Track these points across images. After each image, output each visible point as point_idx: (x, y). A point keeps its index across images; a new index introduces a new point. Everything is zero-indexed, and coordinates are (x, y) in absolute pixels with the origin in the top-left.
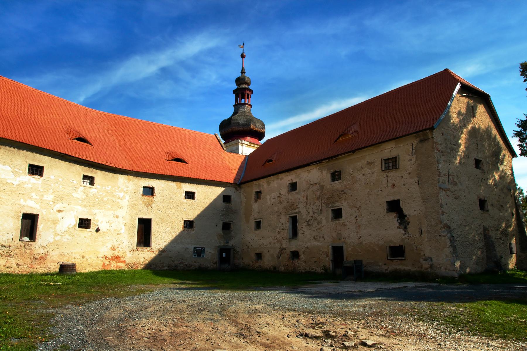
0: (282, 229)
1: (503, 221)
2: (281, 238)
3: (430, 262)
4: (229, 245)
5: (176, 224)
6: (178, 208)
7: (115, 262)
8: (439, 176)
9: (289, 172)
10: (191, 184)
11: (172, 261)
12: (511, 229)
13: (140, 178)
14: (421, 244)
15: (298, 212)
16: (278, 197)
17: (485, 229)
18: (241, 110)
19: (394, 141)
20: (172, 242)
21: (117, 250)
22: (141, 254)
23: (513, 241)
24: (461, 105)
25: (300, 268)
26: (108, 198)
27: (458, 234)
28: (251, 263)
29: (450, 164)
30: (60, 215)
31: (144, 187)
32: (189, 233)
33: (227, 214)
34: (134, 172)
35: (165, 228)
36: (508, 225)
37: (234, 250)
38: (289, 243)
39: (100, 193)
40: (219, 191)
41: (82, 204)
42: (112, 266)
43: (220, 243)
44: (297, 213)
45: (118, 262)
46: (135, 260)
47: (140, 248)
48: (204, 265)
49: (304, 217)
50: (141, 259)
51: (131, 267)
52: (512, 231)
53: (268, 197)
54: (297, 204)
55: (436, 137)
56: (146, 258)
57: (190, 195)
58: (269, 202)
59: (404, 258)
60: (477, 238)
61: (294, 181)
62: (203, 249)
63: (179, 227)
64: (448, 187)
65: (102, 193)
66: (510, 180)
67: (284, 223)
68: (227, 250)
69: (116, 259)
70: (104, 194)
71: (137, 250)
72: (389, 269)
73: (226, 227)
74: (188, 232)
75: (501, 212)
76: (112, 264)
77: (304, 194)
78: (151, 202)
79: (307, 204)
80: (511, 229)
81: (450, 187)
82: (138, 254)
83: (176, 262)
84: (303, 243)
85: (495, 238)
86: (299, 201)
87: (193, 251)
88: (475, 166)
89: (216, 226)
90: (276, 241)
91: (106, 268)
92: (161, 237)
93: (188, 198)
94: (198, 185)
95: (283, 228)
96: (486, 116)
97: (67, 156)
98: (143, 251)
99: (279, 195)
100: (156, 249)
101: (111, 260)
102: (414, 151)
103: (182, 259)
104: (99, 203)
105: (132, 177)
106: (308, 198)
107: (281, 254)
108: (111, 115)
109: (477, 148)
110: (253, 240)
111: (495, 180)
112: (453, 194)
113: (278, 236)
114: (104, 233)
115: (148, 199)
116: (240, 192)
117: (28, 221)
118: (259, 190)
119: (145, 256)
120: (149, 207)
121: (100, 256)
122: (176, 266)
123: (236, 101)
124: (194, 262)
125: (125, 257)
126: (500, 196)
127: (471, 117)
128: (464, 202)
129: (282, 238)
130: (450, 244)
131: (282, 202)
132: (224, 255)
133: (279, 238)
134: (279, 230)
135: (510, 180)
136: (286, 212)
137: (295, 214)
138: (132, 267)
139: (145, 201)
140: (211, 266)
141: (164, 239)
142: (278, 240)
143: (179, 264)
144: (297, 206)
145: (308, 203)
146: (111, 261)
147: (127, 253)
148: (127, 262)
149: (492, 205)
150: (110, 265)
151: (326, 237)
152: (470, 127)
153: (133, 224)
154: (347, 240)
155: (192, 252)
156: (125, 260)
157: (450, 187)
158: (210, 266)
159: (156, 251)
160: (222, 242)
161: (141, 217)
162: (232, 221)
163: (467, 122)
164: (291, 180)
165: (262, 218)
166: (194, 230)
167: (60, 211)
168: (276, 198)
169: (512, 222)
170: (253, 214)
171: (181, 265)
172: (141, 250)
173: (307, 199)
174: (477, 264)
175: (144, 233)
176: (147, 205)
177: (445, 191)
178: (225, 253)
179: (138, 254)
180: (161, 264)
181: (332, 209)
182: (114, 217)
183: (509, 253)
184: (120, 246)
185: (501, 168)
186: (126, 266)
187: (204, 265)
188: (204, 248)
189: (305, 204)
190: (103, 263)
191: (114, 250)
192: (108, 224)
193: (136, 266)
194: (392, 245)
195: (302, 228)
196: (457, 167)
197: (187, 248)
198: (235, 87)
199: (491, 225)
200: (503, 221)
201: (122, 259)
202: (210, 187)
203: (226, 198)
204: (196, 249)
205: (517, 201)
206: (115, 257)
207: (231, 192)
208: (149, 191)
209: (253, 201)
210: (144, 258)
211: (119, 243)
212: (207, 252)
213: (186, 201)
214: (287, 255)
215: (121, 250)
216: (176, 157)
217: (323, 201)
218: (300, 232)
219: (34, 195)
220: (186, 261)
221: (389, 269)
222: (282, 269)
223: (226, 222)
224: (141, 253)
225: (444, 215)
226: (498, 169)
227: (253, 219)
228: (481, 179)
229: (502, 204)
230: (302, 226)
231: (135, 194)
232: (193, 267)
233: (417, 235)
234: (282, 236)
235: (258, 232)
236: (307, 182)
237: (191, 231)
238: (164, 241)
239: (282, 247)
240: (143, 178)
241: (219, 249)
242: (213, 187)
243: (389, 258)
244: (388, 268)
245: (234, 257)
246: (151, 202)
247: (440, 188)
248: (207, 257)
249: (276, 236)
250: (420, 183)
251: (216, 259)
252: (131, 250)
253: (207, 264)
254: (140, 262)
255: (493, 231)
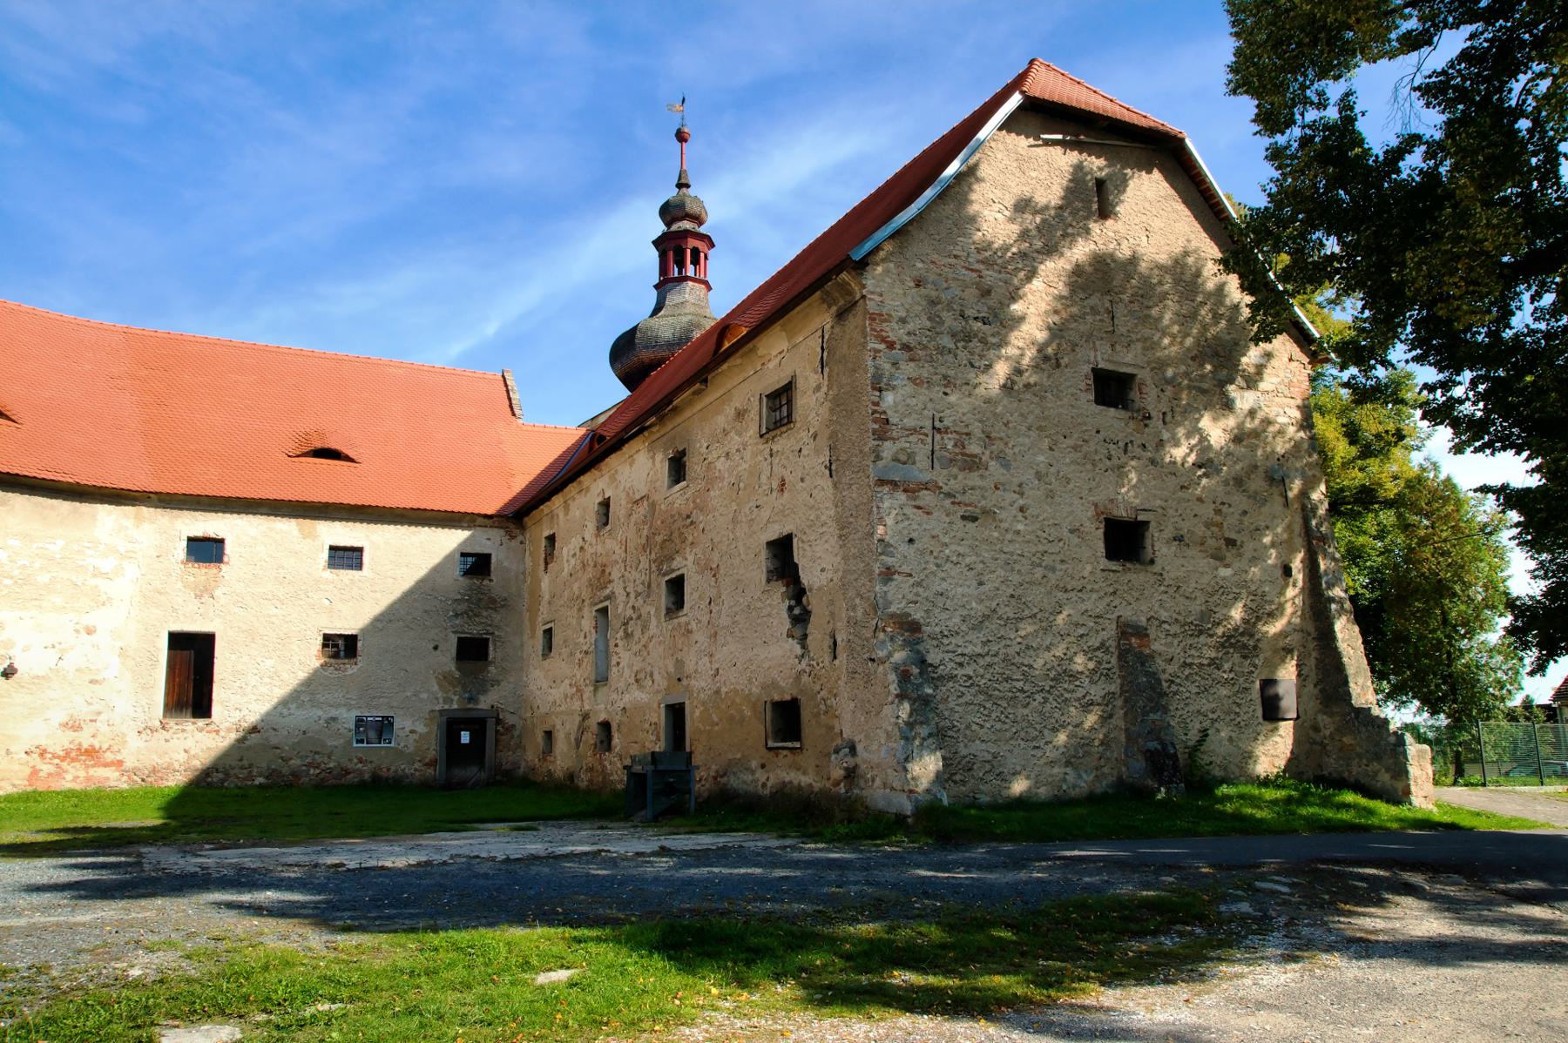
1: (1231, 596)
3: (846, 760)
4: (480, 707)
5: (295, 647)
6: (303, 596)
7: (78, 767)
8: (881, 436)
10: (350, 524)
11: (282, 758)
12: (1274, 628)
13: (176, 512)
14: (835, 691)
17: (1128, 631)
18: (673, 298)
19: (777, 328)
20: (284, 703)
21: (88, 731)
22: (175, 740)
23: (1287, 674)
24: (1034, 174)
26: (54, 574)
27: (966, 651)
29: (948, 390)
31: (190, 540)
35: (259, 660)
36: (1261, 611)
37: (498, 721)
39: (20, 563)
40: (450, 540)
42: (69, 777)
43: (447, 700)
45: (93, 766)
46: (155, 760)
47: (171, 722)
48: (393, 769)
50: (176, 756)
51: (139, 781)
52: (1283, 634)
55: (881, 295)
56: (192, 752)
57: (346, 557)
59: (797, 745)
60: (1080, 662)
63: (310, 658)
64: (926, 477)
65: (27, 563)
66: (1288, 446)
68: (477, 724)
69: (83, 758)
70: (37, 565)
71: (163, 728)
72: (769, 784)
73: (473, 651)
75: (1227, 566)
76: (66, 772)
78: (213, 584)
80: (1274, 628)
81: (940, 476)
82: (167, 741)
83: (295, 762)
85: (1185, 665)
88: (1092, 397)
91: (41, 787)
92: (244, 686)
94: (372, 526)
96: (1176, 211)
98: (183, 731)
100: (227, 724)
101: (62, 761)
102: (825, 354)
103: (316, 753)
104: (18, 590)
105: (152, 510)
109: (1111, 329)
111: (1204, 445)
112: (953, 503)
114: (36, 681)
115: (202, 572)
116: (522, 543)
117: (189, 655)
119: (190, 743)
120: (206, 598)
121: (18, 749)
122: (295, 774)
123: (664, 270)
124: (355, 761)
125: (119, 751)
126: (1223, 504)
127: (1087, 218)
128: (1018, 532)
130: (898, 691)
132: (465, 737)
135: (1292, 443)
138: (143, 780)
139: (193, 579)
140: (417, 773)
141: (255, 691)
143: (304, 768)
147: (128, 739)
148: (128, 764)
149: (1179, 539)
150: (60, 773)
151: (656, 676)
152: (1080, 251)
153: (152, 649)
154: (693, 682)
155: (350, 730)
156: (119, 757)
157: (940, 476)
158: (412, 774)
159: (229, 730)
160: (456, 698)
163: (1064, 236)
166: (356, 664)
169: (1282, 599)
171: (312, 771)
174: (1068, 763)
175: (192, 677)
176: (199, 593)
177: (905, 491)
179: (167, 741)
180: (242, 768)
181: (667, 578)
182: (77, 631)
183: (1261, 720)
184: (100, 718)
185: (1244, 400)
186: (125, 778)
187: (393, 769)
190: (28, 771)
191: (75, 731)
192: (53, 655)
193: (160, 775)
194: (777, 698)
196: (988, 401)
197: (334, 719)
198: (659, 228)
199: (1164, 615)
200: (1231, 596)
201: (109, 757)
203: (477, 565)
204: (363, 721)
205: (1314, 523)
207: (490, 542)
208: (206, 550)
210: (186, 751)
211: (94, 708)
212: (403, 728)
213: (330, 574)
215: (104, 728)
216: (319, 445)
217: (653, 556)
220: (329, 757)
221: (769, 784)
224: (175, 736)
225: (894, 583)
226: (1228, 405)
228: (1121, 444)
229: (1233, 536)
231: (161, 559)
232: (352, 775)
233: (827, 658)
236: (628, 494)
237: (348, 666)
238: (254, 697)
240: (185, 512)
241: (444, 719)
242: (426, 528)
243: (771, 744)
244: (768, 779)
245: (496, 745)
246: (213, 584)
247: (881, 482)
248: (402, 745)
250: (833, 468)
251: (433, 749)
252: (141, 729)
253: (403, 767)
254: (170, 764)
255: (1175, 635)
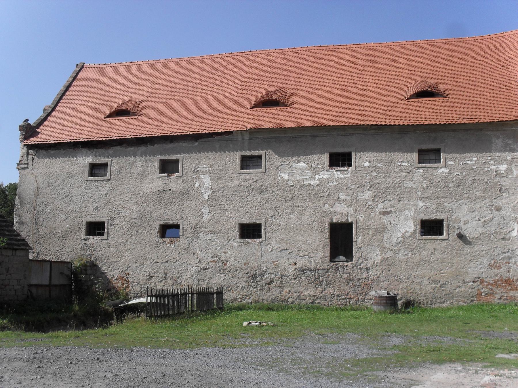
30: (385, 219)
41: (423, 196)
97: (394, 126)
146: (494, 288)
167: (385, 213)
206: (502, 280)
219: (343, 197)
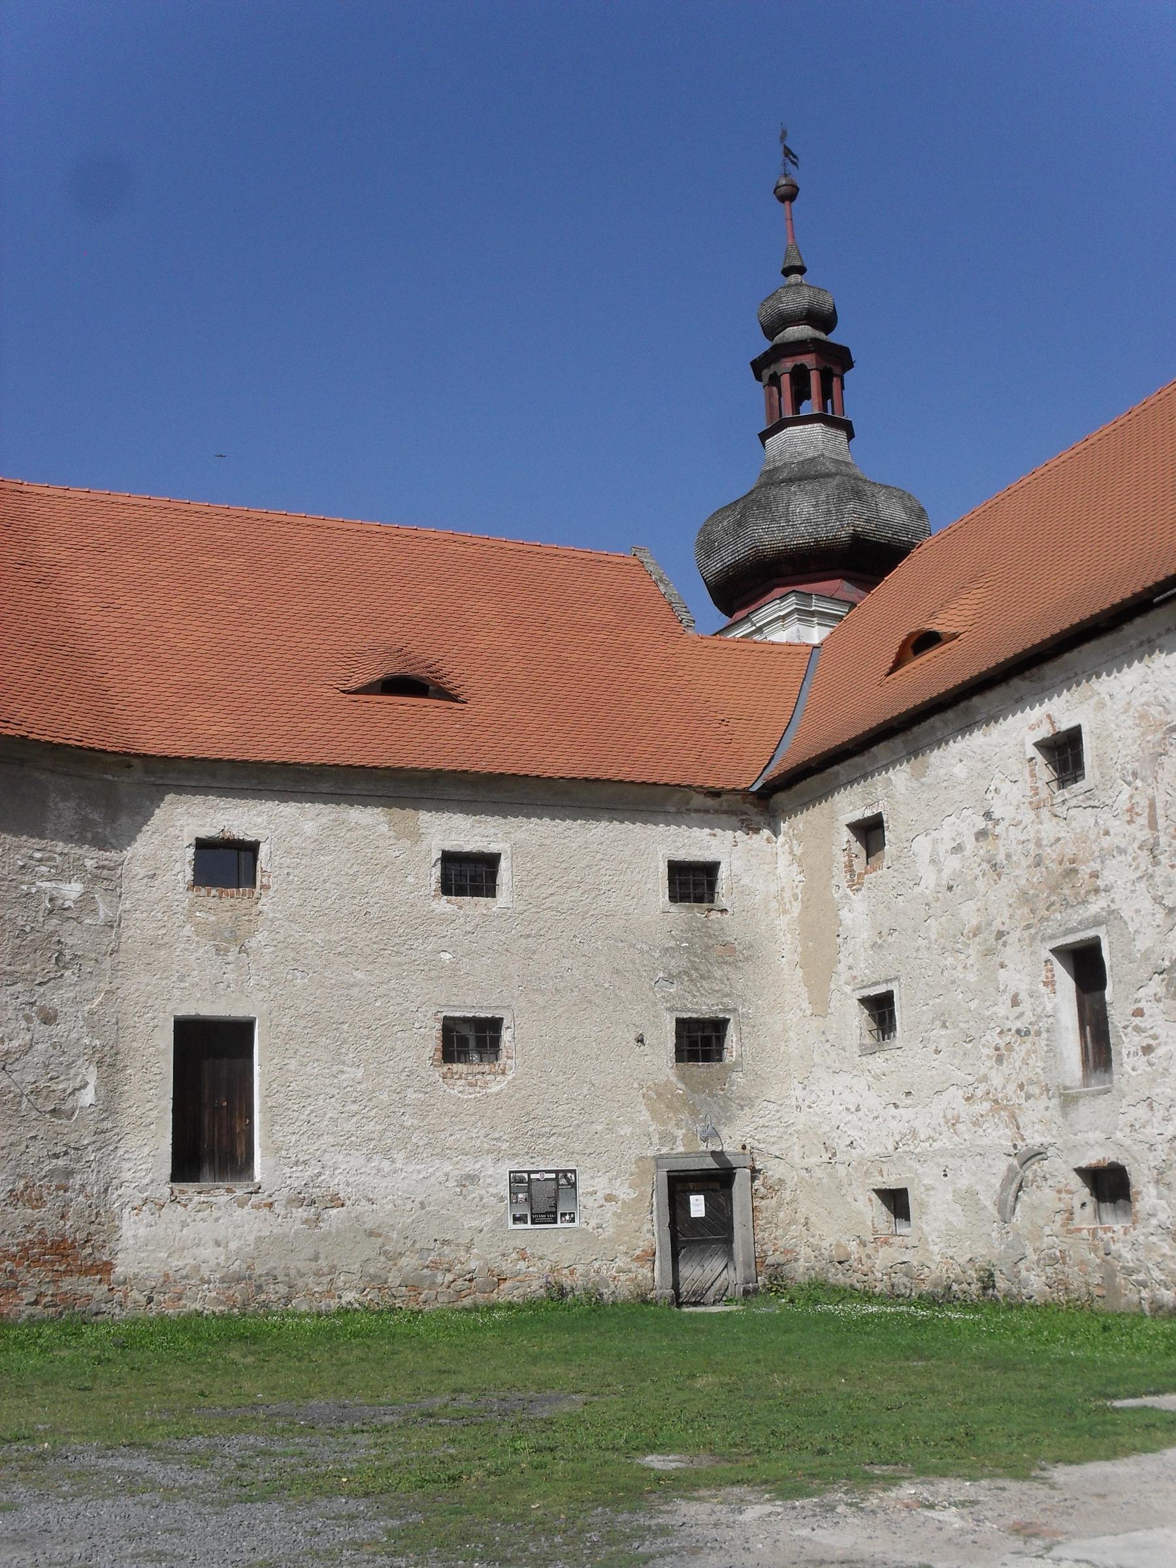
0: (1018, 1031)
2: (1012, 1087)
9: (1027, 674)
15: (1111, 916)
16: (982, 835)
25: (1141, 1277)
28: (853, 1246)
31: (202, 845)
32: (478, 1089)
33: (696, 970)
34: (135, 761)
38: (1065, 1115)
42: (28, 1296)
44: (1097, 922)
45: (68, 1272)
48: (580, 1269)
49: (1142, 944)
53: (922, 846)
54: (1095, 866)
58: (930, 878)
61: (1064, 725)
62: (565, 1177)
67: (1023, 996)
74: (470, 1085)
77: (1131, 797)
79: (1156, 862)
84: (1152, 1109)
86: (1106, 842)
87: (506, 1193)
89: (640, 1040)
90: (986, 1105)
93: (461, 892)
95: (1019, 1024)
98: (211, 1205)
99: (981, 824)
103: (445, 1242)
106: (1161, 822)
107: (1020, 1188)
108: (61, 493)
110: (858, 1109)
113: (997, 1080)
118: (869, 813)
129: (1021, 1087)
131: (1005, 862)
133: (1004, 1088)
134: (998, 1040)
136: (1028, 927)
137: (1087, 928)
142: (996, 1101)
144: (1095, 875)
145: (1161, 849)
161: (190, 1009)
162: (735, 1010)
164: (1046, 722)
165: (896, 978)
168: (970, 843)
170: (845, 960)
172: (196, 1198)
173: (1153, 824)
178: (702, 1197)
187: (580, 1269)
188: (574, 1171)
189: (1144, 857)
195: (1139, 1013)
197: (472, 1178)
202: (631, 826)
206: (43, 1243)
209: (842, 878)
213: (445, 905)
214: (1059, 1192)
218: (1125, 1043)
222: (1035, 1283)
223: (695, 1016)
227: (848, 989)
230: (1137, 1001)
234: (1022, 1078)
235: (877, 1062)
239: (1019, 1143)
249: (985, 1079)
